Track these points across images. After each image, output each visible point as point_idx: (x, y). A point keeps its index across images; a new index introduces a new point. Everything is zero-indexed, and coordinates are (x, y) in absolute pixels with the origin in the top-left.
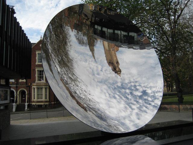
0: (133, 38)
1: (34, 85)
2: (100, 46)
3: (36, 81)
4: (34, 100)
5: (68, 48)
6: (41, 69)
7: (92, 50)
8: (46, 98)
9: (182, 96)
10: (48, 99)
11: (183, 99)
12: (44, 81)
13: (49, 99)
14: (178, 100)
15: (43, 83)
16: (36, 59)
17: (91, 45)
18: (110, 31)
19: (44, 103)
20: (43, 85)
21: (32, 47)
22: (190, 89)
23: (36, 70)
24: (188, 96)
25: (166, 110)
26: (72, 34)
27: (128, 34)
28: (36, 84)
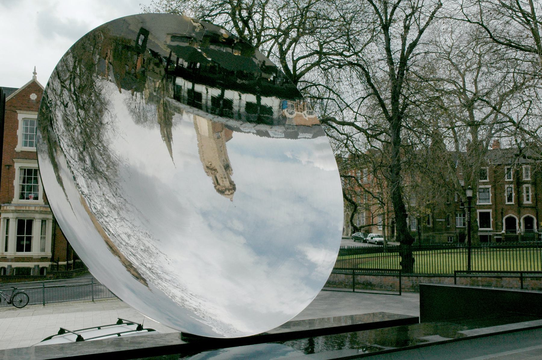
0: (269, 110)
1: (6, 211)
2: (191, 127)
3: (16, 199)
4: (6, 253)
5: (108, 135)
6: (31, 165)
7: (168, 138)
8: (43, 250)
9: (411, 255)
10: (48, 253)
11: (413, 260)
12: (41, 201)
13: (53, 251)
14: (401, 264)
15: (35, 205)
16: (16, 137)
17: (166, 124)
18: (215, 92)
19: (37, 263)
20: (36, 212)
21: (7, 99)
22: (446, 235)
23: (17, 166)
24: (448, 253)
25: (370, 289)
26: (118, 100)
27: (259, 99)
28: (13, 208)
